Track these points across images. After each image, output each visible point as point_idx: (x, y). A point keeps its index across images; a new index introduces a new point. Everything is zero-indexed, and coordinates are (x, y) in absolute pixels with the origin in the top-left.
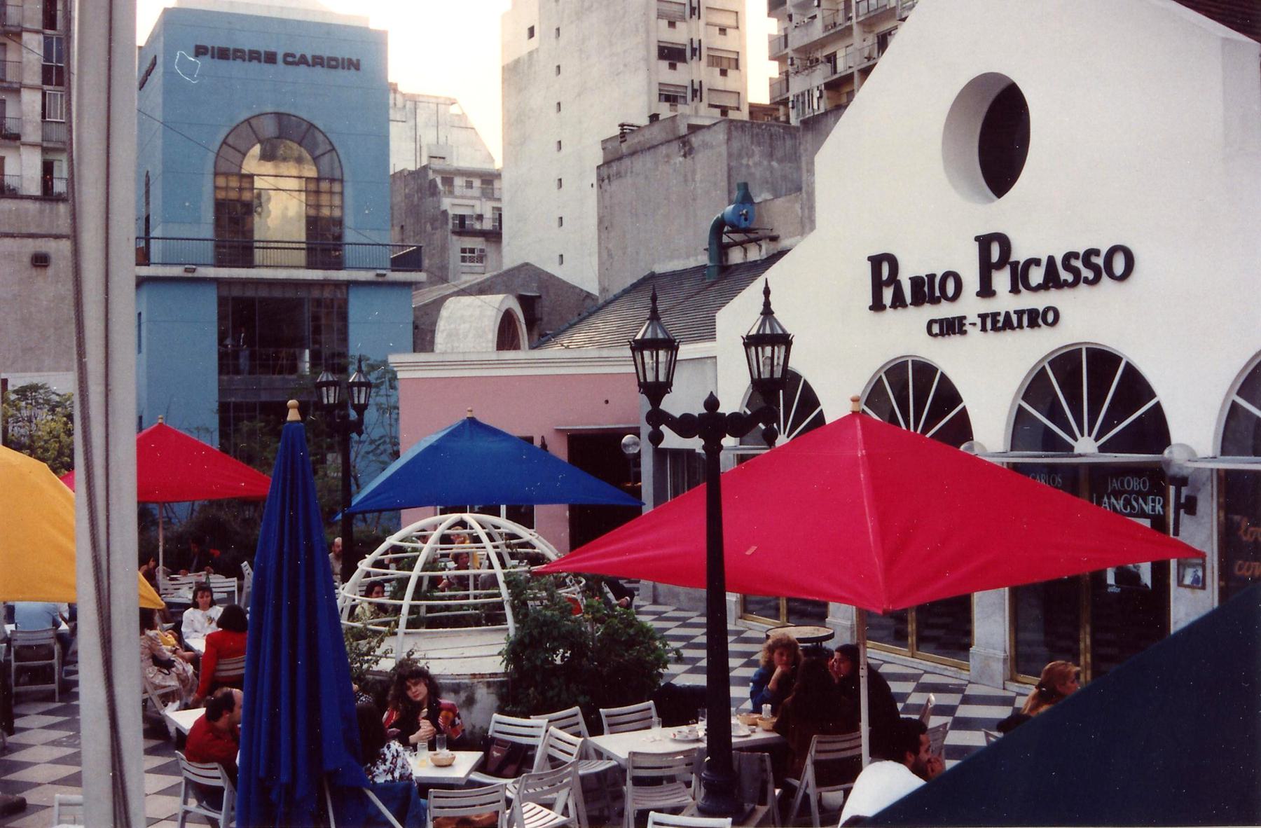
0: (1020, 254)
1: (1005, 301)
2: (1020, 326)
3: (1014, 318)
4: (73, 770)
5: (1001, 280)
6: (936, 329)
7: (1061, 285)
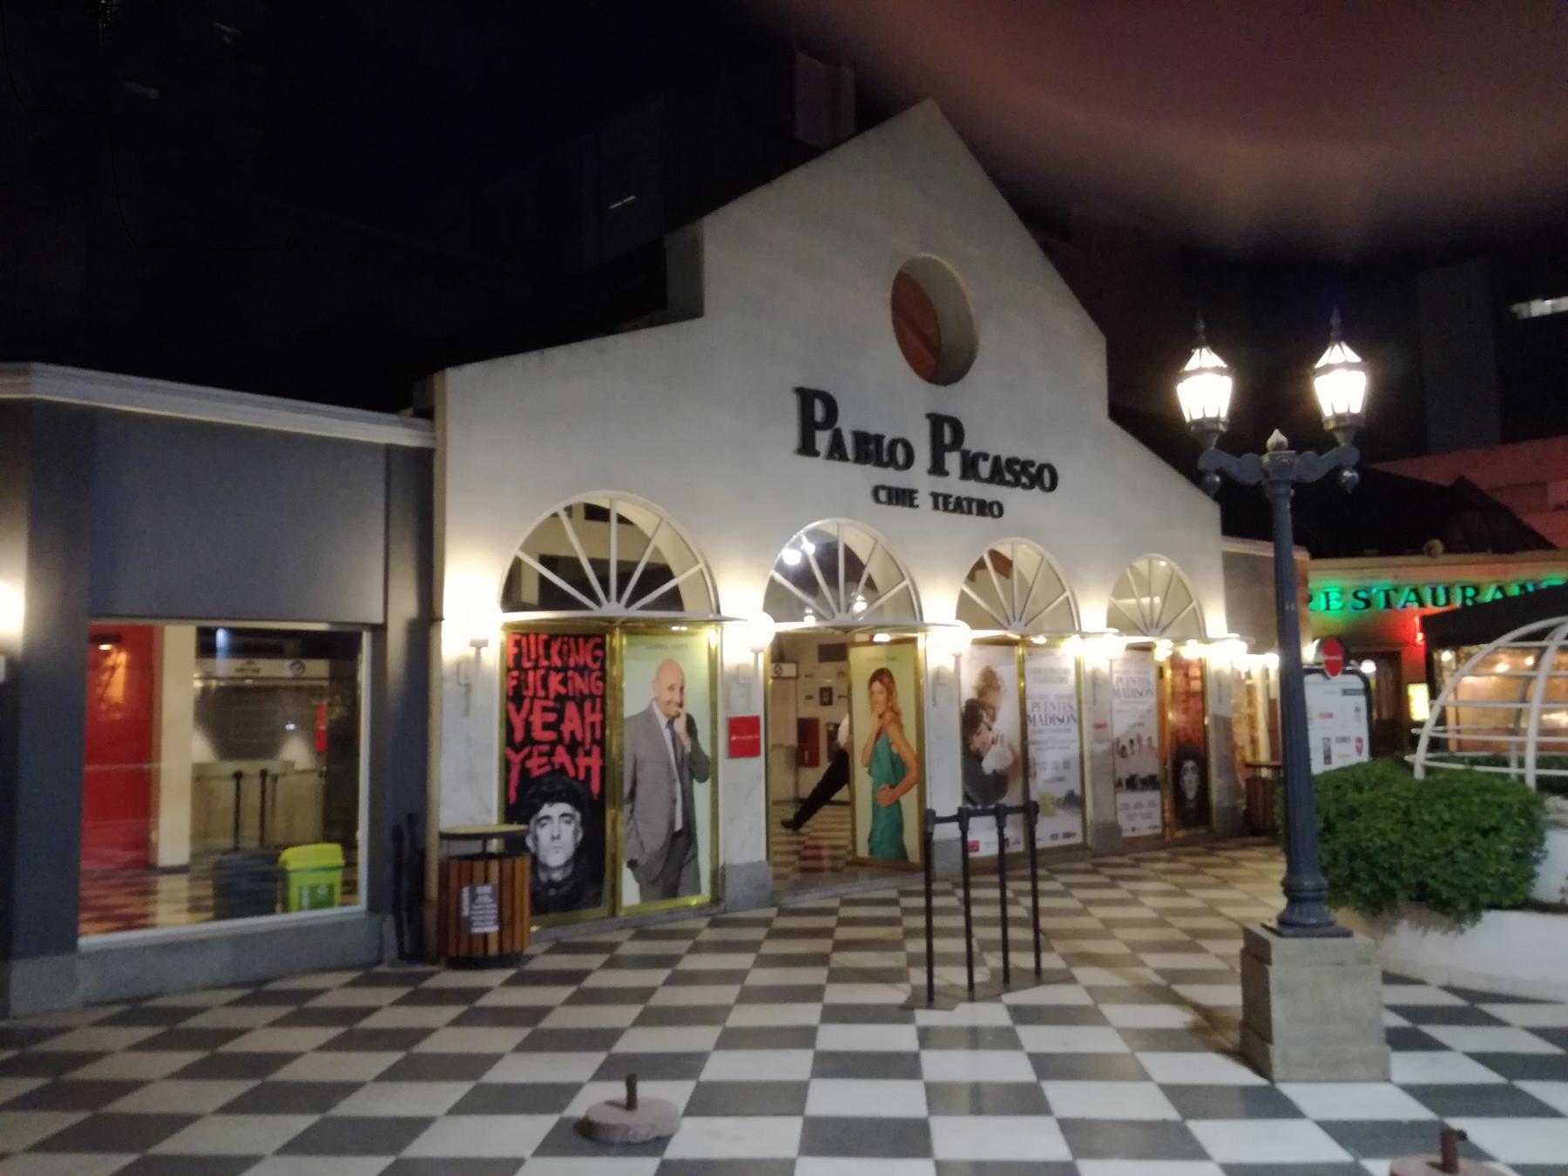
0: (971, 444)
1: (954, 484)
2: (970, 512)
3: (965, 503)
4: (941, 500)
5: (953, 461)
6: (883, 495)
7: (1003, 482)
